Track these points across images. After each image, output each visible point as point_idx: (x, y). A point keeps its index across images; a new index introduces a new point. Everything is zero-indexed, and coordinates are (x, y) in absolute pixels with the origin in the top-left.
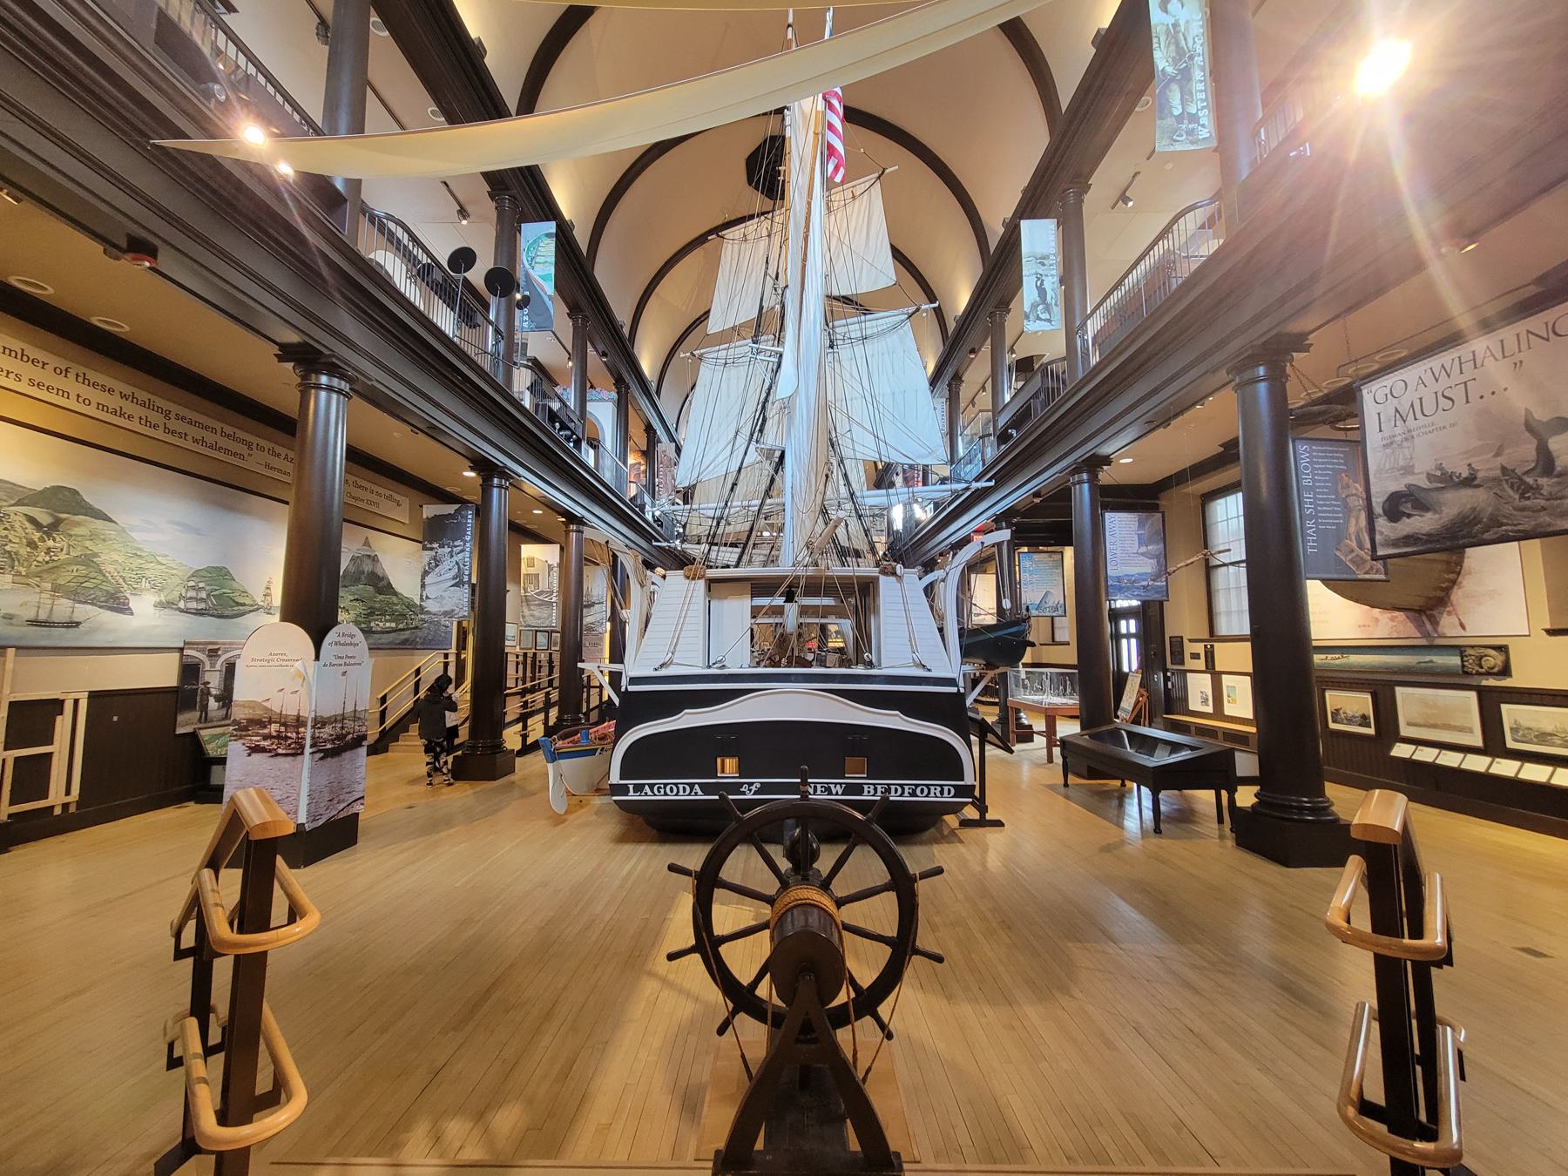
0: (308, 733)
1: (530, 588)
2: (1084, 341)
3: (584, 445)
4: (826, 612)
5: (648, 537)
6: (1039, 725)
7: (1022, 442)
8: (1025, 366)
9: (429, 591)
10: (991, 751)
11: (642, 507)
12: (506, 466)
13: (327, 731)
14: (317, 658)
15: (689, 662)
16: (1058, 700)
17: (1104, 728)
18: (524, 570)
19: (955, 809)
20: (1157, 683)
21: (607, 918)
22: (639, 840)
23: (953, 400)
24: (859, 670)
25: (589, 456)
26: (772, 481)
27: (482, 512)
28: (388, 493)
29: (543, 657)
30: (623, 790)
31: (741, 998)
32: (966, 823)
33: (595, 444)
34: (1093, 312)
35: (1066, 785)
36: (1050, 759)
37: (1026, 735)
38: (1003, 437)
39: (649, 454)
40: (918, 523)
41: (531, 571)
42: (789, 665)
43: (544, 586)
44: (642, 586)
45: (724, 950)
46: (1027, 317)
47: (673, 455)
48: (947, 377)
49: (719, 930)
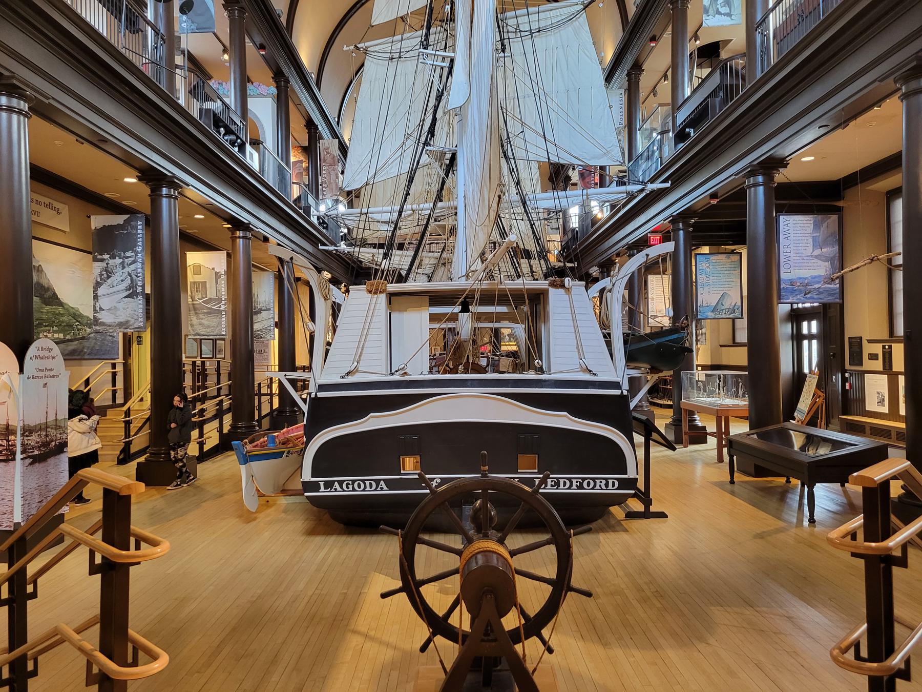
0: (18, 440)
1: (198, 296)
2: (765, 36)
3: (248, 148)
4: (500, 317)
5: (314, 240)
6: (711, 427)
7: (705, 137)
8: (709, 53)
9: (103, 302)
10: (657, 451)
11: (307, 210)
12: (174, 176)
13: (34, 439)
14: (21, 371)
15: (374, 369)
16: (729, 402)
17: (771, 428)
18: (191, 278)
19: (619, 500)
20: (835, 385)
21: (310, 593)
22: (328, 532)
23: (632, 91)
24: (530, 375)
25: (252, 158)
26: (443, 183)
27: (152, 222)
28: (47, 201)
29: (210, 366)
30: (315, 487)
31: (438, 625)
32: (631, 515)
33: (256, 143)
34: (774, 8)
35: (732, 482)
36: (720, 459)
37: (699, 436)
38: (681, 136)
39: (310, 150)
40: (594, 221)
41: (198, 279)
42: (466, 371)
43: (211, 293)
44: (326, 299)
45: (423, 589)
46: (706, 11)
47: (336, 152)
48: (625, 66)
49: (419, 576)
